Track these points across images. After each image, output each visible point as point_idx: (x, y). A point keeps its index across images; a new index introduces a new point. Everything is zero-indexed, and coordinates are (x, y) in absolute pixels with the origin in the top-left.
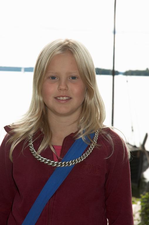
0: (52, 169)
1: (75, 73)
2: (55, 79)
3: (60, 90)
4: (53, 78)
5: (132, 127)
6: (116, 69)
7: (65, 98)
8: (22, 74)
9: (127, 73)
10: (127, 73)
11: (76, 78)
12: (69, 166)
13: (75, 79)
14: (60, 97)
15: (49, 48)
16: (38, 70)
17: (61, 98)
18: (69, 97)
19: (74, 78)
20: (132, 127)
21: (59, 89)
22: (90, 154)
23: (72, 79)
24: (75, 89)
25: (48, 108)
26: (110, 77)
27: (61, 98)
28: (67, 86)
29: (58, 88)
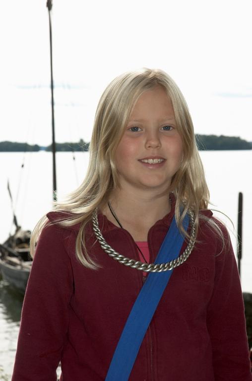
0: (140, 278)
1: (168, 122)
2: (137, 131)
3: (149, 148)
4: (135, 129)
5: (241, 196)
6: (50, 154)
7: (156, 161)
8: (42, 153)
9: (36, 148)
10: (36, 148)
11: (171, 128)
12: (159, 265)
13: (169, 129)
14: (147, 159)
15: (134, 105)
16: (107, 116)
17: (151, 161)
18: (161, 158)
19: (167, 128)
20: (241, 196)
21: (148, 145)
22: (190, 255)
23: (164, 130)
24: (170, 146)
25: (129, 125)
26: (59, 140)
27: (151, 161)
28: (160, 143)
29: (146, 143)
